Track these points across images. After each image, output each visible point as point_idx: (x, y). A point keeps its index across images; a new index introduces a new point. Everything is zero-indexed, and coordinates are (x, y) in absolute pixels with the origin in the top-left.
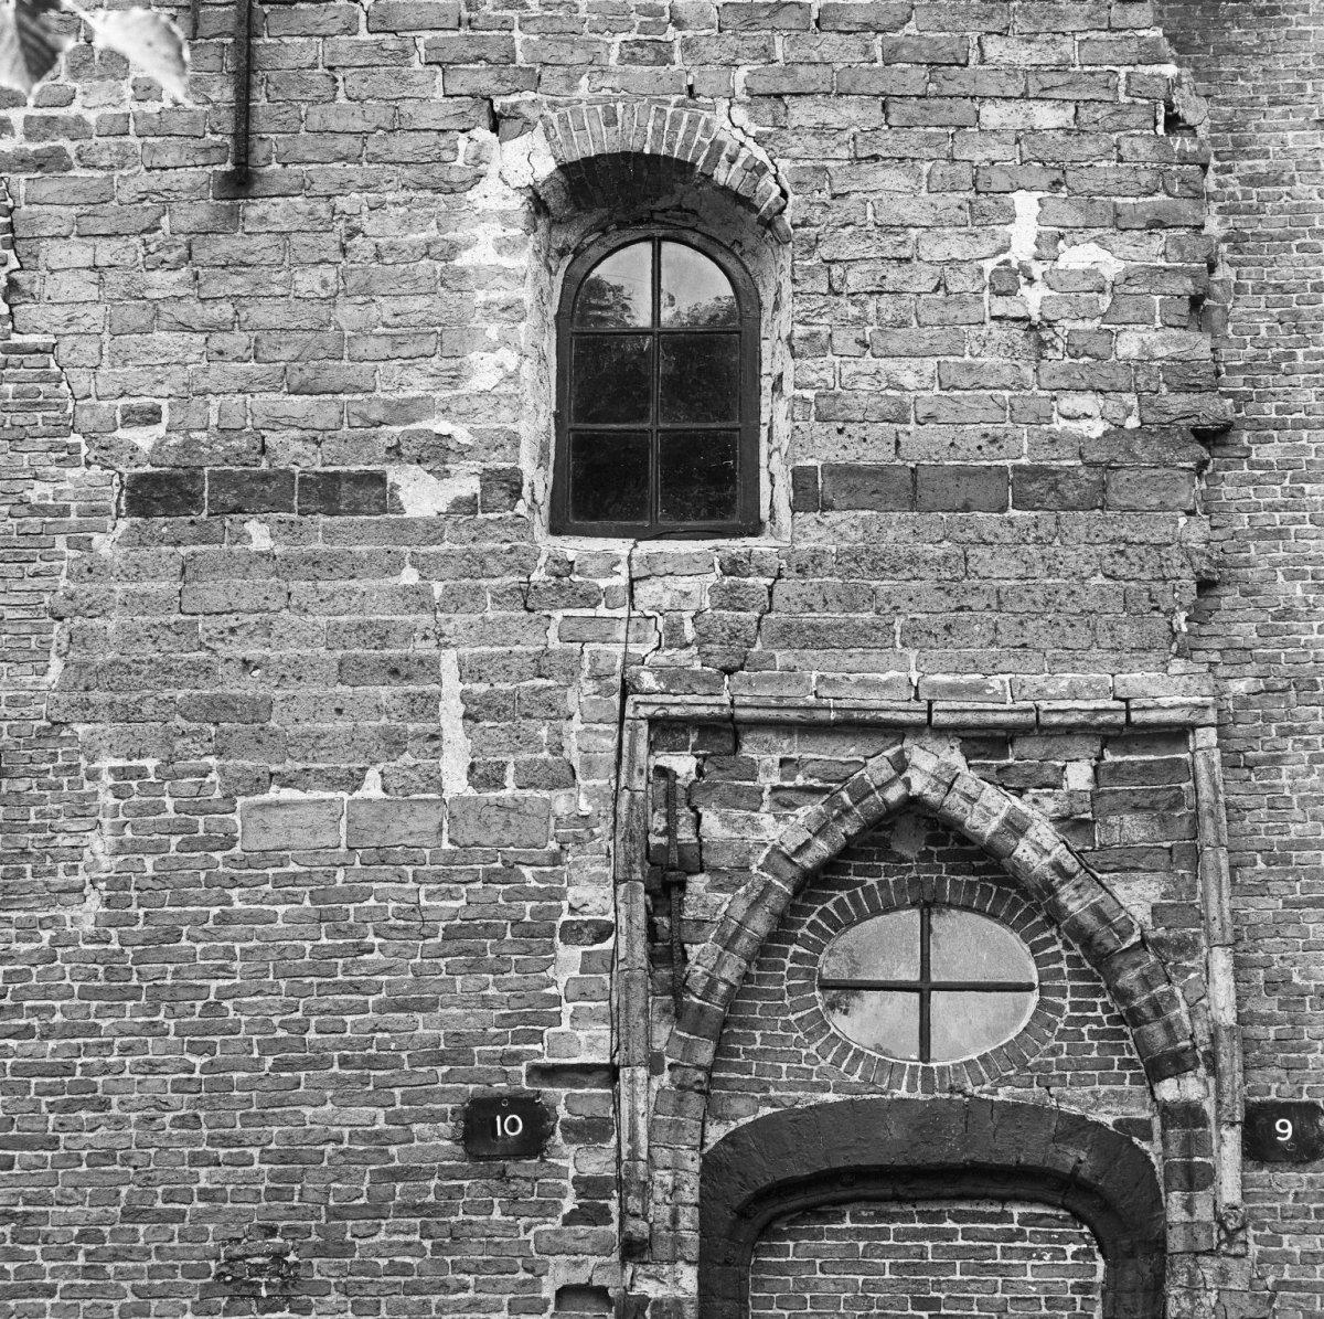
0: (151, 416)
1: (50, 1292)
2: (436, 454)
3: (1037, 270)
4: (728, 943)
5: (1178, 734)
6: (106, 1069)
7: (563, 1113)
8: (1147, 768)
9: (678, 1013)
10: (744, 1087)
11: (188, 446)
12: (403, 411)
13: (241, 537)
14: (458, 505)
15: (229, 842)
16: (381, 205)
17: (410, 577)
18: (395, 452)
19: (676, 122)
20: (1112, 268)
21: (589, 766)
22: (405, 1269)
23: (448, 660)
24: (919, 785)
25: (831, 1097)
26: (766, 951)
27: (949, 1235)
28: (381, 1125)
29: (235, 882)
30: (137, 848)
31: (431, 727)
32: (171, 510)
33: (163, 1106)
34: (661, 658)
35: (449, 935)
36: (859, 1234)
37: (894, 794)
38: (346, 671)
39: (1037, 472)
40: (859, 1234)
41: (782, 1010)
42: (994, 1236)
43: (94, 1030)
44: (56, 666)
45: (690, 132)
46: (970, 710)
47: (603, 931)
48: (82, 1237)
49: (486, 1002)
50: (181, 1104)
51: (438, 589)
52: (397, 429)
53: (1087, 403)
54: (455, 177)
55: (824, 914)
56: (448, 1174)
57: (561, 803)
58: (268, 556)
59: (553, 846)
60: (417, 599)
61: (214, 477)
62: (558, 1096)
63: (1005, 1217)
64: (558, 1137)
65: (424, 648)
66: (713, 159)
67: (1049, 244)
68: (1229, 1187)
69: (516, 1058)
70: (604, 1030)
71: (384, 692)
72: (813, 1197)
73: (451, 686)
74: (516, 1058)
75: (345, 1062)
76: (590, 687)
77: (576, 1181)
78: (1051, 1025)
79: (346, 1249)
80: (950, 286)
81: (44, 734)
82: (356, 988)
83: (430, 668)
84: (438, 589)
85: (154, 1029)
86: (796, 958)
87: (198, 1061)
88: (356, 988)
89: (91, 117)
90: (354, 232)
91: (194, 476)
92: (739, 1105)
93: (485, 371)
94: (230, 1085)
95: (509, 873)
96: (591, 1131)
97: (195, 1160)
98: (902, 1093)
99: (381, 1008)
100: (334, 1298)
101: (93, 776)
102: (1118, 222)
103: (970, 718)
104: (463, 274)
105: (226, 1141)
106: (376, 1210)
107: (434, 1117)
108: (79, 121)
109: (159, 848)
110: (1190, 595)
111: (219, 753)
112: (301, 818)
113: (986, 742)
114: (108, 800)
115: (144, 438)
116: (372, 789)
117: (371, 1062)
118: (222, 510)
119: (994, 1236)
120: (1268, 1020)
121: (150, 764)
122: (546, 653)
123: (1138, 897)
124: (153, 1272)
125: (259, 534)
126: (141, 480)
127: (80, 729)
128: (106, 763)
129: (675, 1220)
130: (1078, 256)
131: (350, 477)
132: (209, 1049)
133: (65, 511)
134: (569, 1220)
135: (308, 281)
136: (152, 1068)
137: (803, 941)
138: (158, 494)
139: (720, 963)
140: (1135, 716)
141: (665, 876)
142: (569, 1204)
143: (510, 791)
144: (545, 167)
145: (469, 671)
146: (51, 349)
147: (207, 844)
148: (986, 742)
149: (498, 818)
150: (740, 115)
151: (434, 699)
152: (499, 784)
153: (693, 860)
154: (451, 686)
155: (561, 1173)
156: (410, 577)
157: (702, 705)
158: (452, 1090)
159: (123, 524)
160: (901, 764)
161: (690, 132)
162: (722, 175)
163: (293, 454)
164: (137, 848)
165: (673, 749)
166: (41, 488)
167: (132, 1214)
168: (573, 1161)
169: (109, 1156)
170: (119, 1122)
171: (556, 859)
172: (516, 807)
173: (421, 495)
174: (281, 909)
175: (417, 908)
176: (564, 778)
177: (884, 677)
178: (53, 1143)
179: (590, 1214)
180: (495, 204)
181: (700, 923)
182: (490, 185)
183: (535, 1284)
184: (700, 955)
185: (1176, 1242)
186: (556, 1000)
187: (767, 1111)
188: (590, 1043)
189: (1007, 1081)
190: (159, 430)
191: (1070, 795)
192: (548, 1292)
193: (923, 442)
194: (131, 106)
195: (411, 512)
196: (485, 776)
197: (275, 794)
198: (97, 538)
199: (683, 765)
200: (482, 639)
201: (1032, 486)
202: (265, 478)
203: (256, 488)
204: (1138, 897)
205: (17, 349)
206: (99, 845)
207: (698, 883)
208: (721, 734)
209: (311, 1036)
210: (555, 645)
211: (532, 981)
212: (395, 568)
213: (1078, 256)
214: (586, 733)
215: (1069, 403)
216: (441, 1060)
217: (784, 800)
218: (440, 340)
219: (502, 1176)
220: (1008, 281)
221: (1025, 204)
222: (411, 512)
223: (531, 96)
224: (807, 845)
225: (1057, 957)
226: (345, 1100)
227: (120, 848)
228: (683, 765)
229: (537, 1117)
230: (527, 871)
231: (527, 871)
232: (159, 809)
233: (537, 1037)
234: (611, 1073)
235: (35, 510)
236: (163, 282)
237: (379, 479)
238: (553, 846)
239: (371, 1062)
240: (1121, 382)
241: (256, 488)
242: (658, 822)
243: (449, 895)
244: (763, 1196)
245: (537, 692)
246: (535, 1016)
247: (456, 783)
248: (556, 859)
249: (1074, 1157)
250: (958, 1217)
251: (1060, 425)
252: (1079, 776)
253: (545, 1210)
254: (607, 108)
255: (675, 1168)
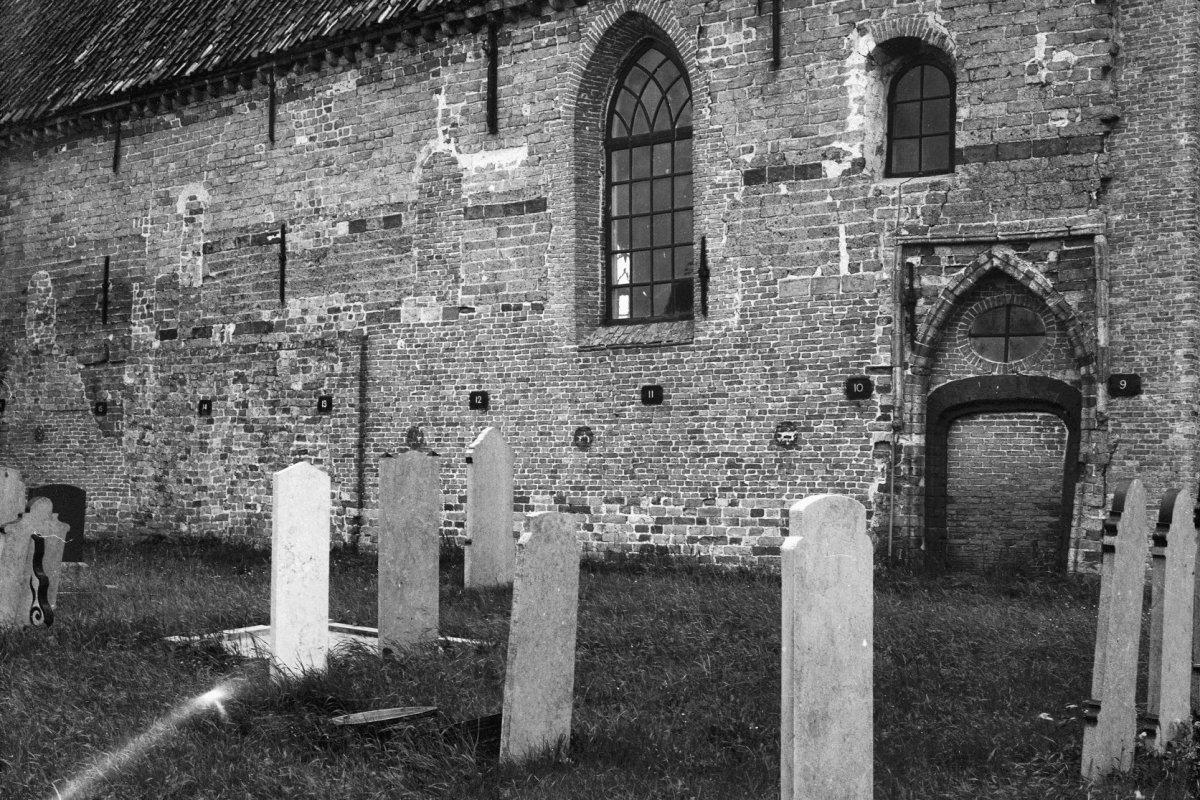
0: (751, 150)
1: (727, 442)
2: (837, 156)
3: (1044, 64)
4: (930, 323)
5: (1090, 237)
6: (741, 371)
7: (876, 383)
8: (1077, 251)
9: (913, 348)
10: (941, 373)
11: (762, 159)
12: (827, 140)
13: (779, 190)
14: (845, 172)
15: (775, 295)
16: (820, 66)
17: (829, 199)
18: (825, 157)
19: (917, 22)
20: (1073, 59)
21: (887, 262)
22: (829, 436)
23: (842, 228)
24: (996, 262)
25: (971, 376)
26: (941, 328)
27: (1014, 423)
28: (822, 388)
29: (778, 308)
30: (749, 297)
31: (836, 252)
32: (757, 183)
33: (758, 382)
34: (909, 223)
35: (843, 323)
36: (984, 423)
37: (987, 267)
38: (812, 234)
39: (1043, 141)
40: (984, 423)
41: (956, 345)
42: (1029, 424)
43: (738, 358)
44: (725, 237)
45: (921, 27)
46: (1013, 234)
47: (889, 321)
48: (736, 425)
49: (853, 346)
50: (763, 382)
51: (838, 203)
52: (825, 147)
53: (1064, 113)
54: (842, 53)
55: (972, 311)
56: (842, 404)
57: (877, 276)
58: (786, 196)
59: (875, 291)
60: (832, 206)
61: (771, 170)
62: (875, 378)
63: (1034, 417)
64: (874, 392)
65: (833, 224)
66: (928, 36)
67: (1049, 54)
68: (1101, 404)
69: (861, 364)
70: (888, 354)
71: (822, 240)
72: (967, 411)
73: (843, 236)
74: (861, 364)
75: (811, 367)
76: (887, 234)
77: (881, 406)
78: (1049, 348)
79: (812, 430)
80: (1028, 74)
81: (722, 261)
82: (814, 342)
83: (835, 231)
84: (838, 203)
85: (754, 358)
86: (961, 327)
87: (768, 368)
88: (814, 342)
89: (731, 47)
90: (812, 77)
91: (763, 169)
92: (940, 379)
93: (854, 122)
94: (776, 376)
95: (861, 302)
96: (885, 389)
97: (768, 400)
98: (995, 373)
99: (822, 349)
100: (808, 445)
101: (736, 275)
102: (1076, 40)
103: (1013, 238)
104: (845, 88)
105: (776, 394)
106: (820, 416)
107: (837, 385)
108: (728, 49)
109: (755, 297)
110: (1098, 184)
111: (772, 265)
112: (798, 284)
113: (1020, 244)
114: (740, 282)
115: (748, 158)
116: (818, 273)
117: (819, 367)
118: (771, 181)
119: (1029, 424)
120: (1121, 344)
121: (752, 269)
122: (873, 223)
123: (1073, 299)
124: (756, 437)
125: (783, 189)
126: (747, 172)
127: (732, 259)
128: (740, 269)
129: (911, 419)
130: (1059, 57)
131: (811, 166)
132: (771, 364)
133: (725, 186)
134: (879, 419)
135: (797, 98)
136: (754, 370)
137: (964, 321)
138: (753, 177)
139: (927, 331)
140: (1073, 233)
141: (908, 299)
142: (879, 414)
143: (861, 272)
144: (872, 46)
145: (848, 231)
146: (721, 130)
147: (768, 296)
148: (1020, 244)
149: (857, 282)
150: (939, 18)
151: (838, 242)
152: (858, 271)
153: (920, 293)
154: (843, 236)
155: (875, 403)
156: (829, 199)
157: (918, 238)
158: (842, 375)
159: (743, 188)
160: (991, 256)
161: (921, 27)
162: (931, 41)
163: (793, 159)
164: (749, 297)
165: (912, 255)
166: (719, 178)
167: (749, 418)
168: (879, 399)
169: (742, 400)
170: (745, 388)
171: (876, 296)
172: (863, 278)
173: (833, 170)
174: (791, 316)
175: (832, 315)
176: (878, 268)
177: (984, 224)
178: (726, 395)
179: (885, 418)
180: (857, 62)
181: (921, 316)
182: (853, 55)
183: (867, 441)
184: (921, 327)
185: (1083, 425)
186: (875, 345)
187: (949, 381)
188: (883, 358)
189: (1033, 368)
190: (752, 155)
191: (1050, 263)
192: (872, 444)
193: (1001, 135)
194: (743, 41)
195: (830, 177)
196: (853, 268)
197: (790, 277)
198: (735, 194)
199: (915, 260)
200: (852, 220)
201: (1042, 148)
202: (785, 168)
203: (783, 172)
204: (1073, 299)
205: (713, 131)
206: (738, 297)
207: (921, 301)
208: (927, 249)
209: (801, 359)
210: (875, 220)
211: (868, 337)
212: (824, 197)
213: (1059, 57)
214: (886, 252)
215: (1054, 114)
216: (839, 366)
217: (950, 269)
218: (837, 116)
219: (859, 405)
220: (1033, 69)
221: (1041, 37)
222: (830, 177)
223: (867, 20)
224: (957, 286)
225: (1052, 323)
226: (810, 380)
227: (744, 298)
228: (915, 260)
229: (868, 386)
230: (867, 300)
231: (867, 300)
232: (755, 284)
233: (868, 357)
234: (889, 370)
235: (718, 186)
236: (755, 102)
237: (820, 165)
238: (875, 291)
239: (819, 367)
240: (1075, 103)
241: (783, 172)
242: (907, 281)
243: (843, 309)
244: (946, 410)
245: (871, 237)
246: (867, 349)
247: (844, 270)
248: (876, 296)
249: (1055, 398)
250: (1019, 417)
251: (1051, 123)
252: (1052, 256)
253: (872, 416)
254: (890, 21)
255: (912, 401)
